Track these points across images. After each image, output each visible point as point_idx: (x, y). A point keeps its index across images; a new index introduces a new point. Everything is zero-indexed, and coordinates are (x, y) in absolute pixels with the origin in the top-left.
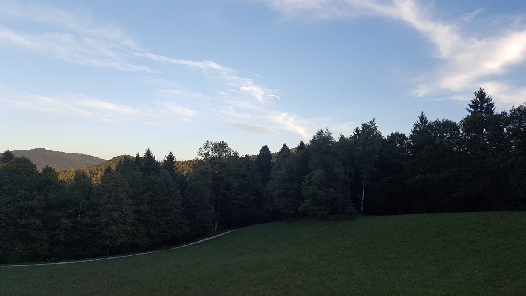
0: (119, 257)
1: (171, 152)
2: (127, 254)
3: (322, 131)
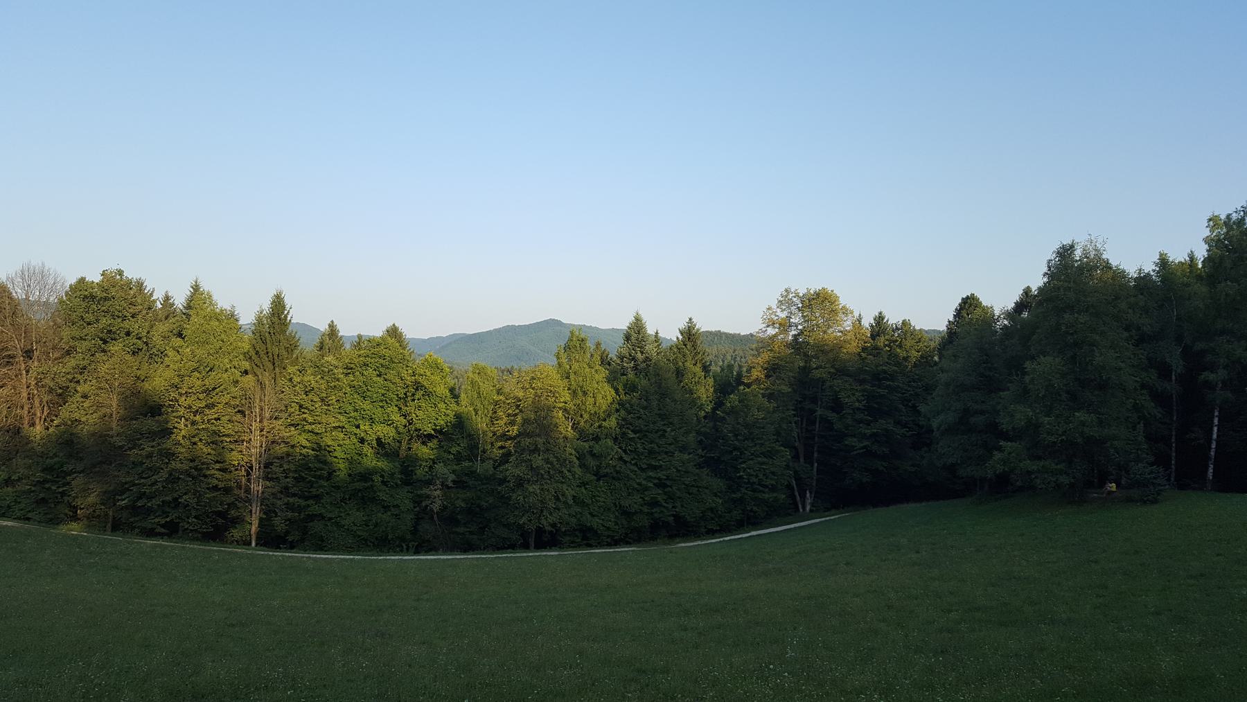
0: (548, 553)
1: (690, 319)
2: (571, 549)
3: (1072, 246)
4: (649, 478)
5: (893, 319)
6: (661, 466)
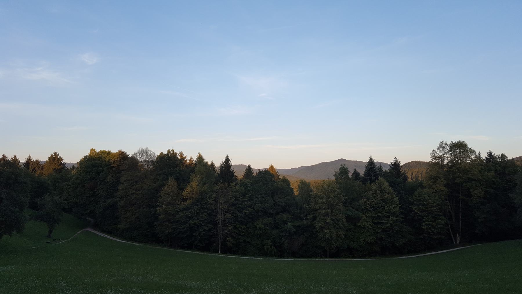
6: (383, 223)
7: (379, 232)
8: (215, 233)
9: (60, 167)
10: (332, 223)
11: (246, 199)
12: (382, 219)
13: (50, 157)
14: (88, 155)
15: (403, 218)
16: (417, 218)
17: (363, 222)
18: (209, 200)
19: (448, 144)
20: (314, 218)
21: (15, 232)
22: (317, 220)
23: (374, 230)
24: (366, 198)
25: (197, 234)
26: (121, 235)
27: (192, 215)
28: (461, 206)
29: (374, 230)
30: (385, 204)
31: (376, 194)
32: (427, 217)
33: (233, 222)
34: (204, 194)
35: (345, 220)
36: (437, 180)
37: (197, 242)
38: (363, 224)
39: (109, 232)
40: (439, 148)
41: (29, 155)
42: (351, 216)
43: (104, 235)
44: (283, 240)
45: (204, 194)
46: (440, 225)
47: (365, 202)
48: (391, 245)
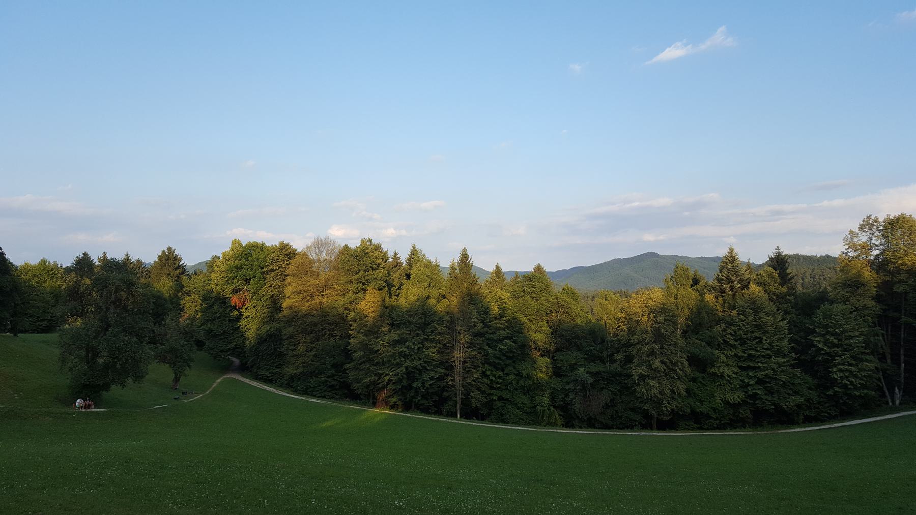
4: (750, 377)
5: (134, 258)
6: (759, 367)
7: (751, 385)
8: (450, 383)
9: (178, 272)
10: (662, 368)
11: (501, 326)
12: (757, 361)
13: (160, 255)
14: (228, 250)
15: (795, 359)
16: (822, 358)
17: (720, 366)
18: (437, 327)
19: (881, 220)
20: (629, 359)
21: (130, 380)
22: (634, 362)
23: (741, 381)
24: (726, 324)
25: (419, 385)
26: (290, 384)
27: (410, 353)
28: (903, 336)
29: (742, 381)
30: (763, 333)
31: (744, 315)
32: (840, 356)
33: (481, 365)
34: (430, 316)
35: (686, 363)
36: (858, 288)
37: (420, 399)
38: (721, 370)
39: (267, 381)
40: (862, 227)
41: (127, 252)
42: (698, 356)
43: (261, 385)
44: (571, 397)
45: (430, 316)
46: (867, 371)
47: (724, 330)
48: (773, 407)
